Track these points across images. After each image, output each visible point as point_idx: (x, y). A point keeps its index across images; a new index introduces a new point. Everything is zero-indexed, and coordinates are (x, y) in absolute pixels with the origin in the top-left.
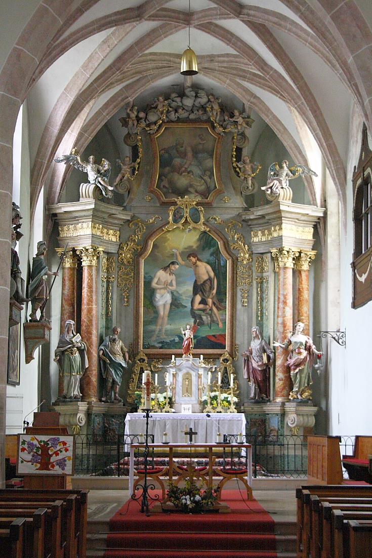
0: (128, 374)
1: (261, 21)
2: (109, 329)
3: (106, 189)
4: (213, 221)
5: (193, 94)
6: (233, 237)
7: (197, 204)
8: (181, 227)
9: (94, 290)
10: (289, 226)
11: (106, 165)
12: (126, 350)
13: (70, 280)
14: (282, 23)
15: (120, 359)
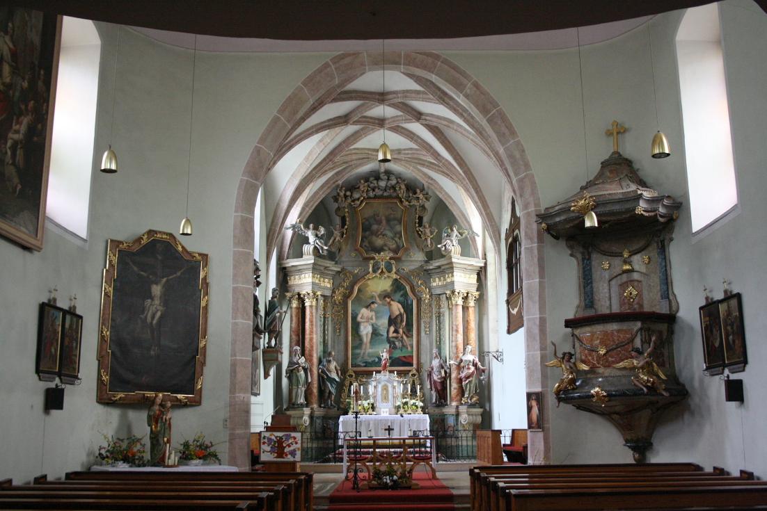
0: (340, 386)
1: (435, 124)
2: (326, 353)
3: (322, 248)
4: (402, 271)
6: (417, 283)
7: (391, 259)
9: (314, 323)
10: (459, 274)
11: (322, 231)
12: (338, 368)
13: (296, 316)
14: (451, 125)
15: (334, 376)
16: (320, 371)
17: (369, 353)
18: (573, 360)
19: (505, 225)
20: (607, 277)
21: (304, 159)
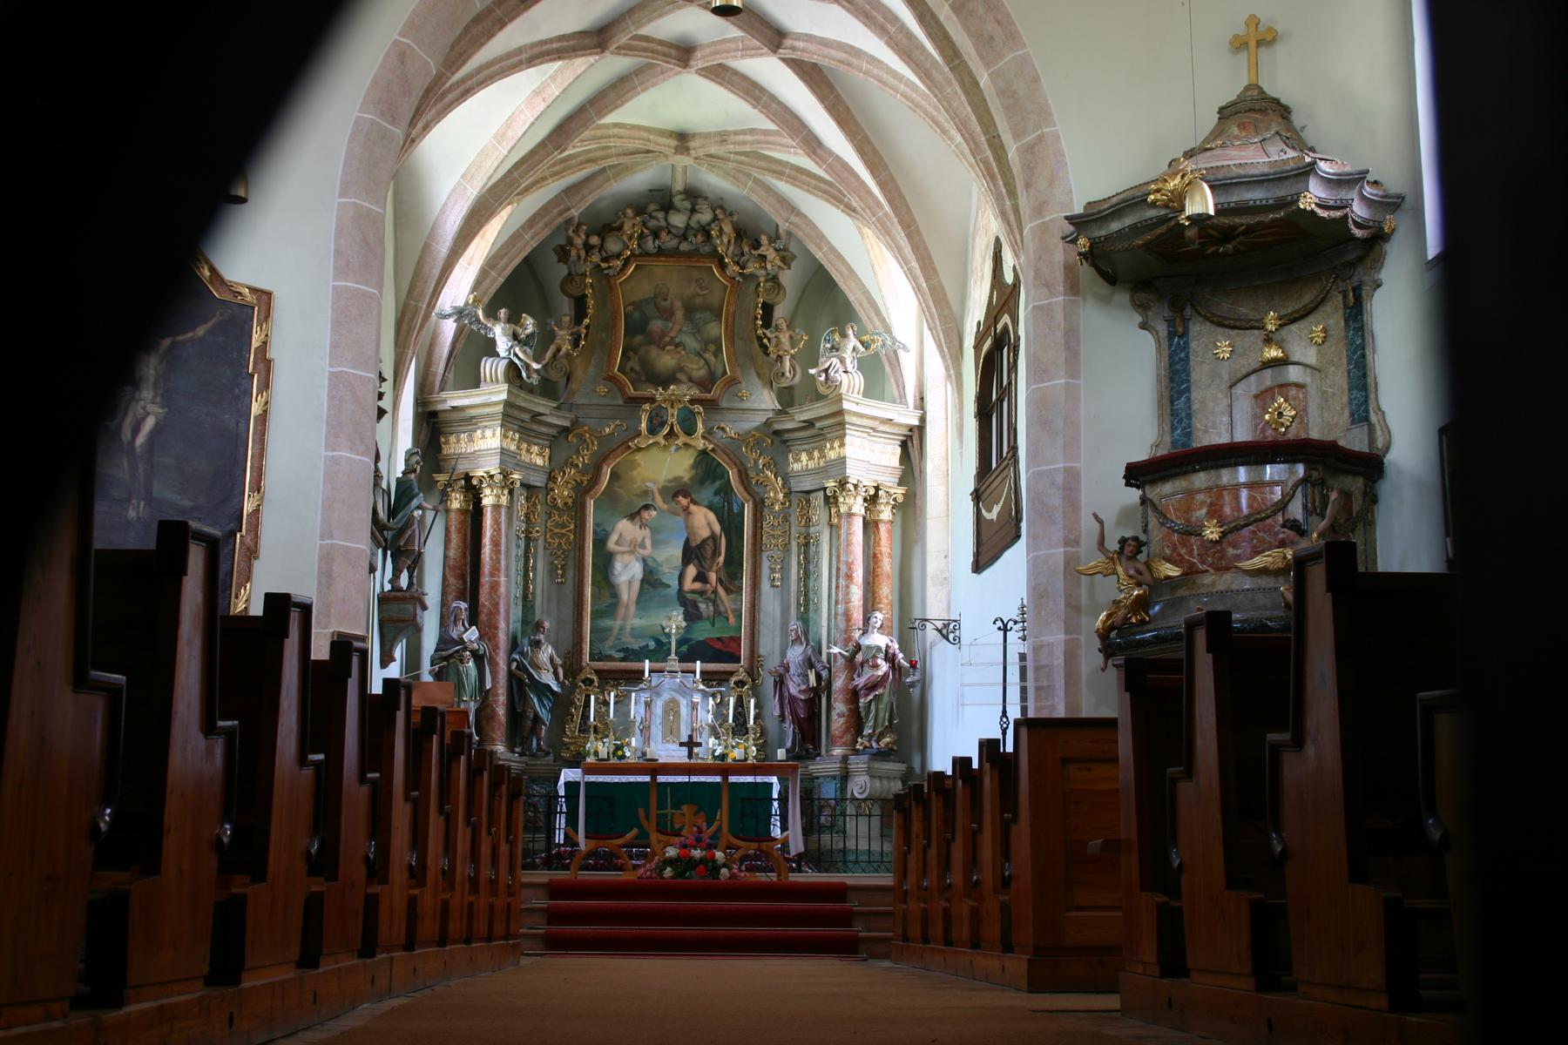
0: (562, 704)
1: (815, 59)
2: (531, 624)
3: (528, 366)
4: (720, 434)
5: (687, 204)
6: (756, 462)
7: (692, 402)
8: (663, 442)
9: (503, 549)
10: (857, 441)
11: (529, 324)
12: (559, 661)
13: (459, 531)
14: (854, 60)
15: (547, 678)
16: (514, 665)
17: (633, 629)
18: (1142, 557)
19: (976, 313)
20: (1226, 377)
21: (495, 137)
